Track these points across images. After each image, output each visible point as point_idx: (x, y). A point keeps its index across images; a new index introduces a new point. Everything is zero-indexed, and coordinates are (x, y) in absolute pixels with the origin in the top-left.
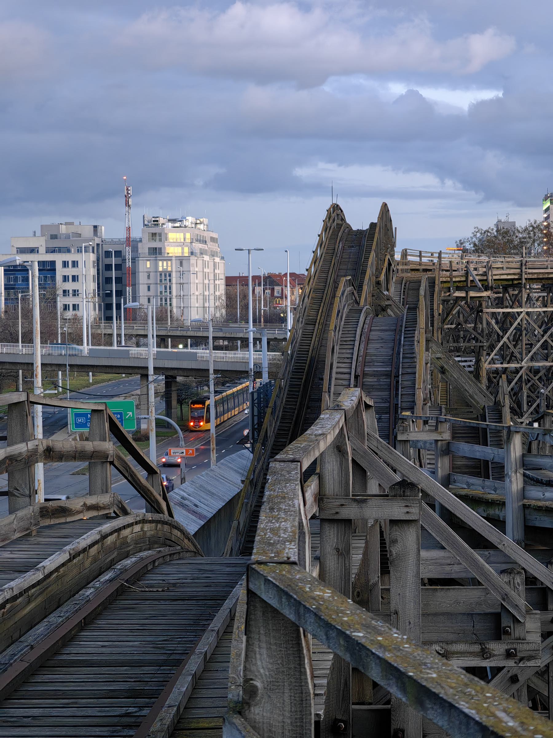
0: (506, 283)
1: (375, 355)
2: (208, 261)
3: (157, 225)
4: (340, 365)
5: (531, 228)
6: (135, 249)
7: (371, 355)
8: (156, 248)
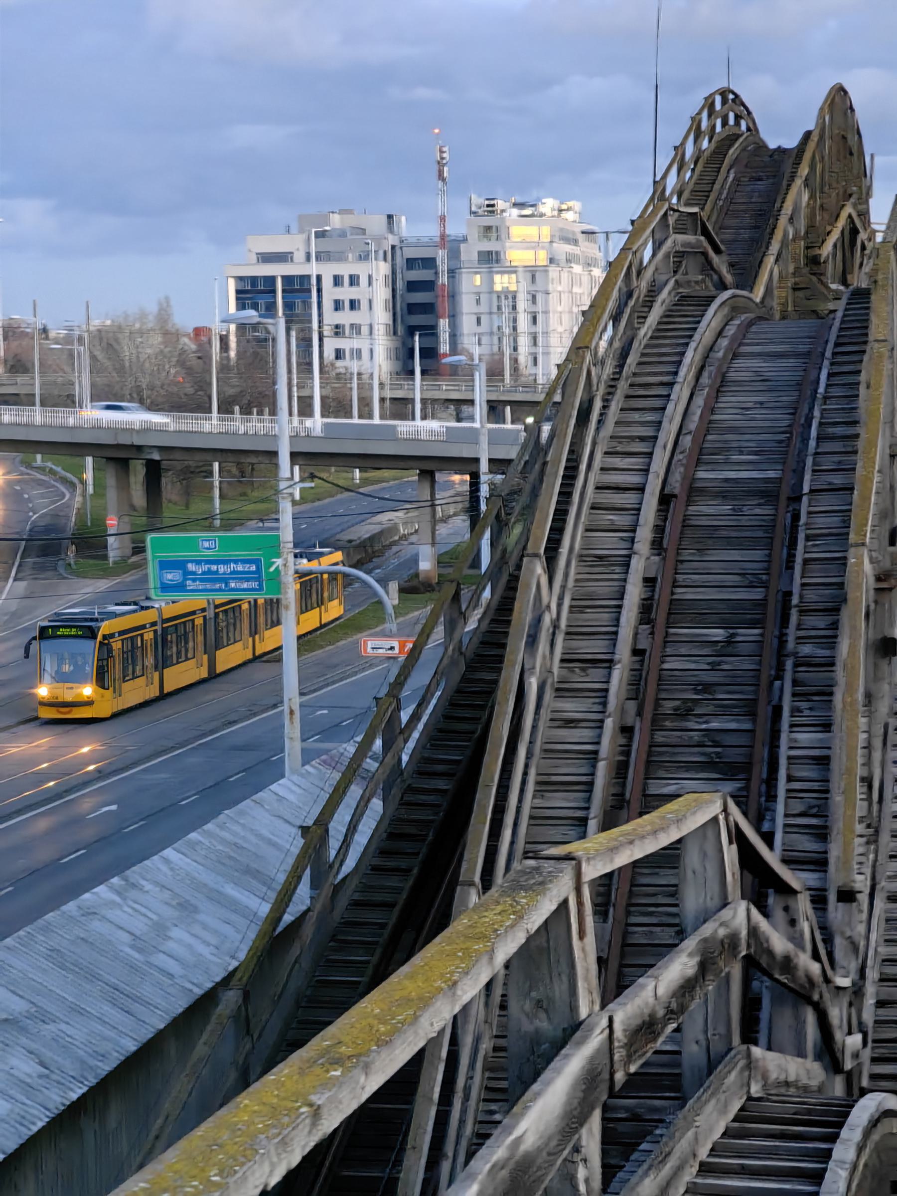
1: (732, 430)
2: (580, 275)
3: (493, 212)
4: (618, 462)
6: (454, 254)
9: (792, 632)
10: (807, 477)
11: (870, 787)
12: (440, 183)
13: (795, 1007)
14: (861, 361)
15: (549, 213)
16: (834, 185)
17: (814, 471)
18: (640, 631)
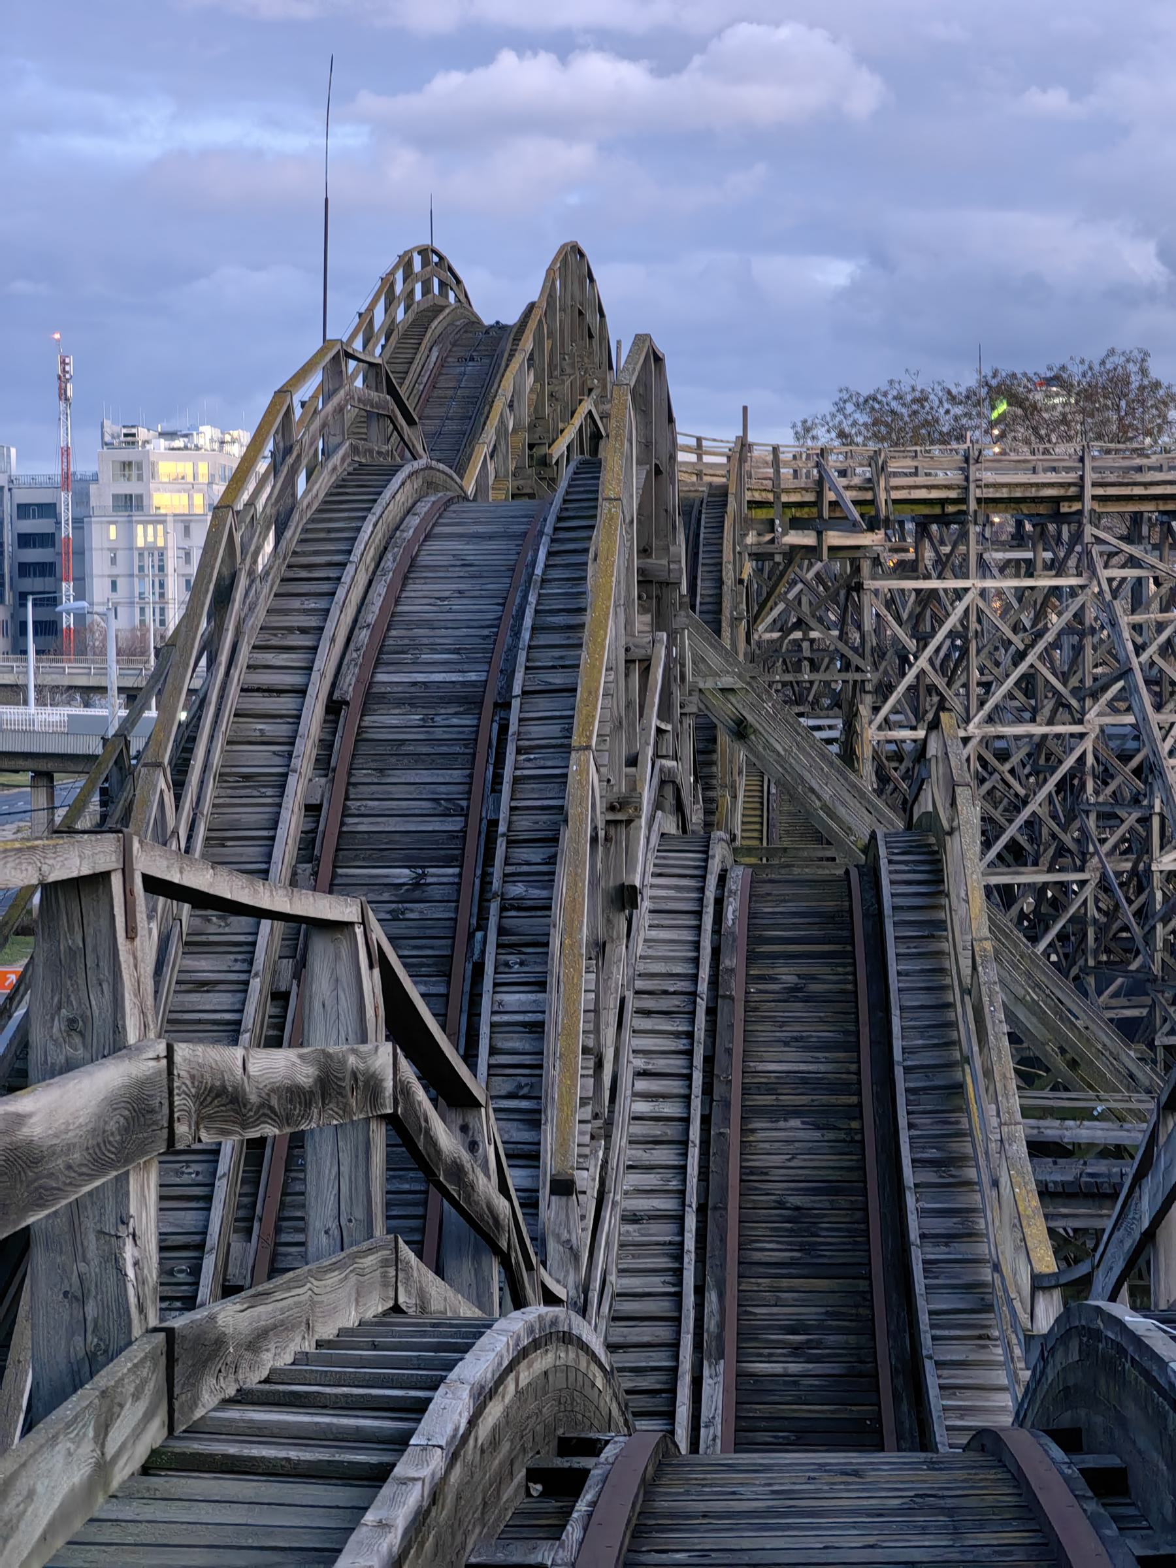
1: (430, 625)
3: (133, 443)
4: (270, 658)
5: (984, 391)
6: (82, 499)
7: (410, 625)
8: (131, 496)
9: (497, 870)
10: (519, 676)
11: (599, 1065)
12: (62, 404)
13: (477, 1257)
14: (590, 538)
15: (208, 447)
16: (568, 370)
17: (527, 668)
18: (299, 871)
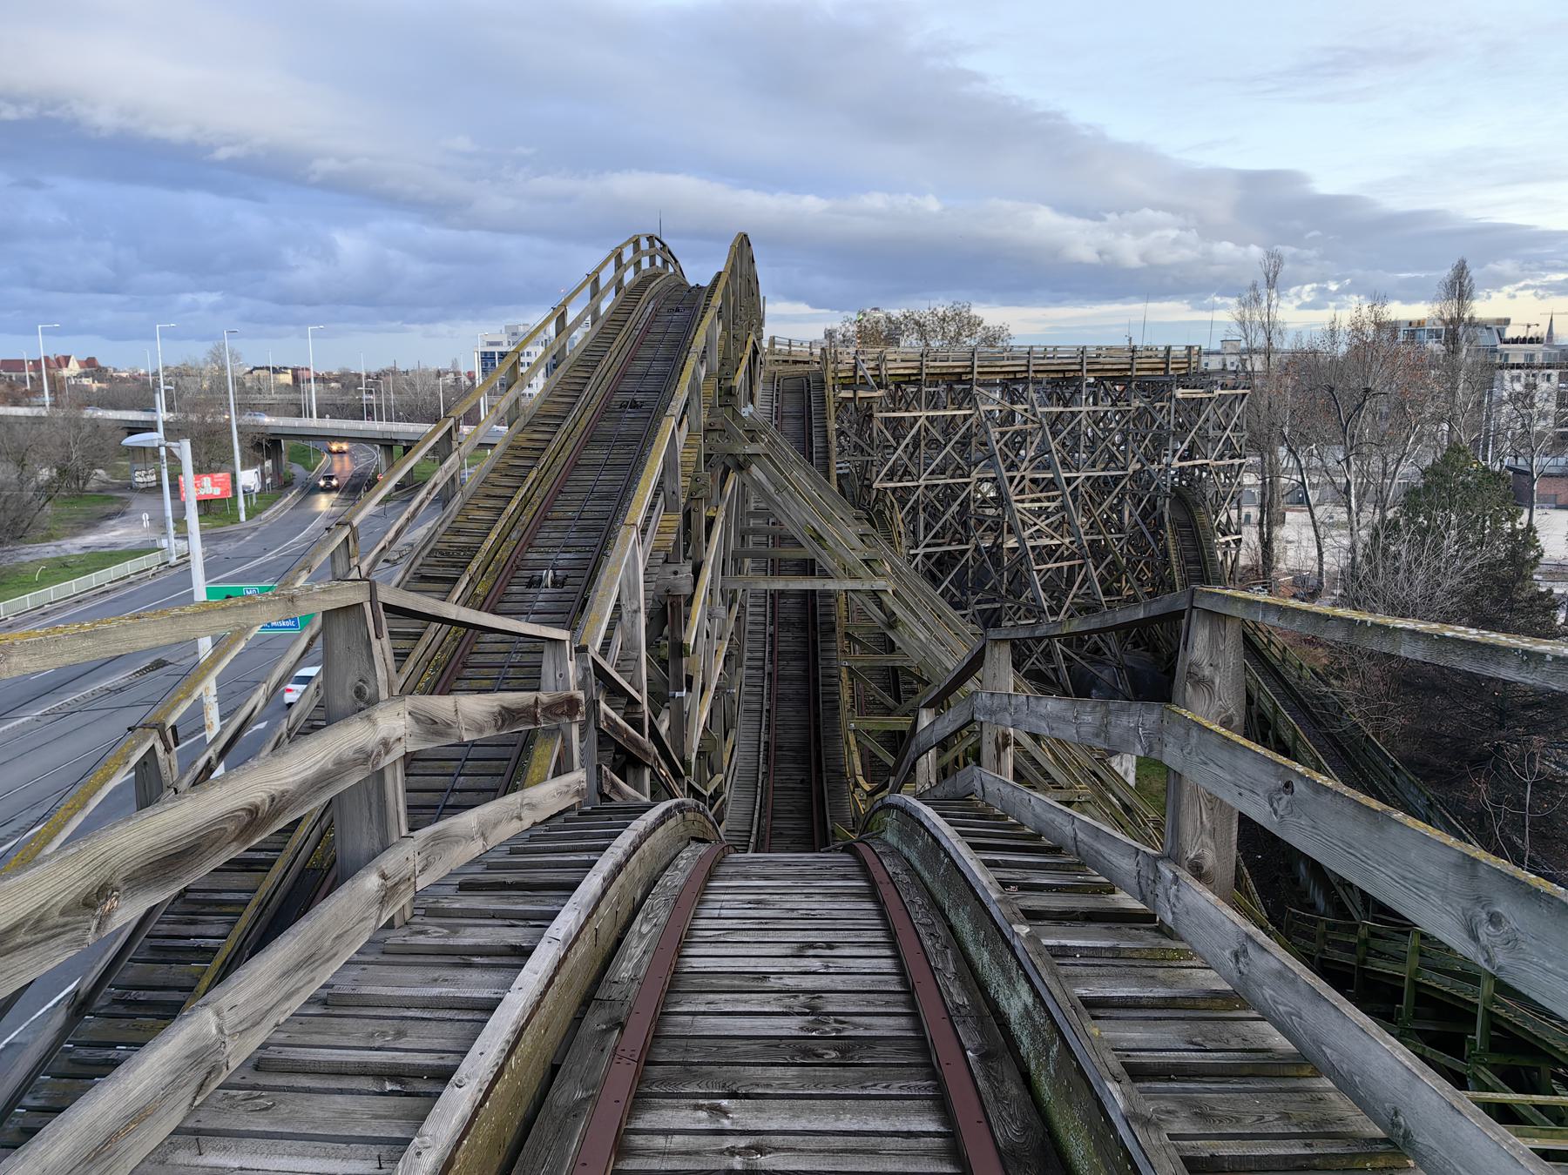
0: (902, 379)
16: (744, 317)
